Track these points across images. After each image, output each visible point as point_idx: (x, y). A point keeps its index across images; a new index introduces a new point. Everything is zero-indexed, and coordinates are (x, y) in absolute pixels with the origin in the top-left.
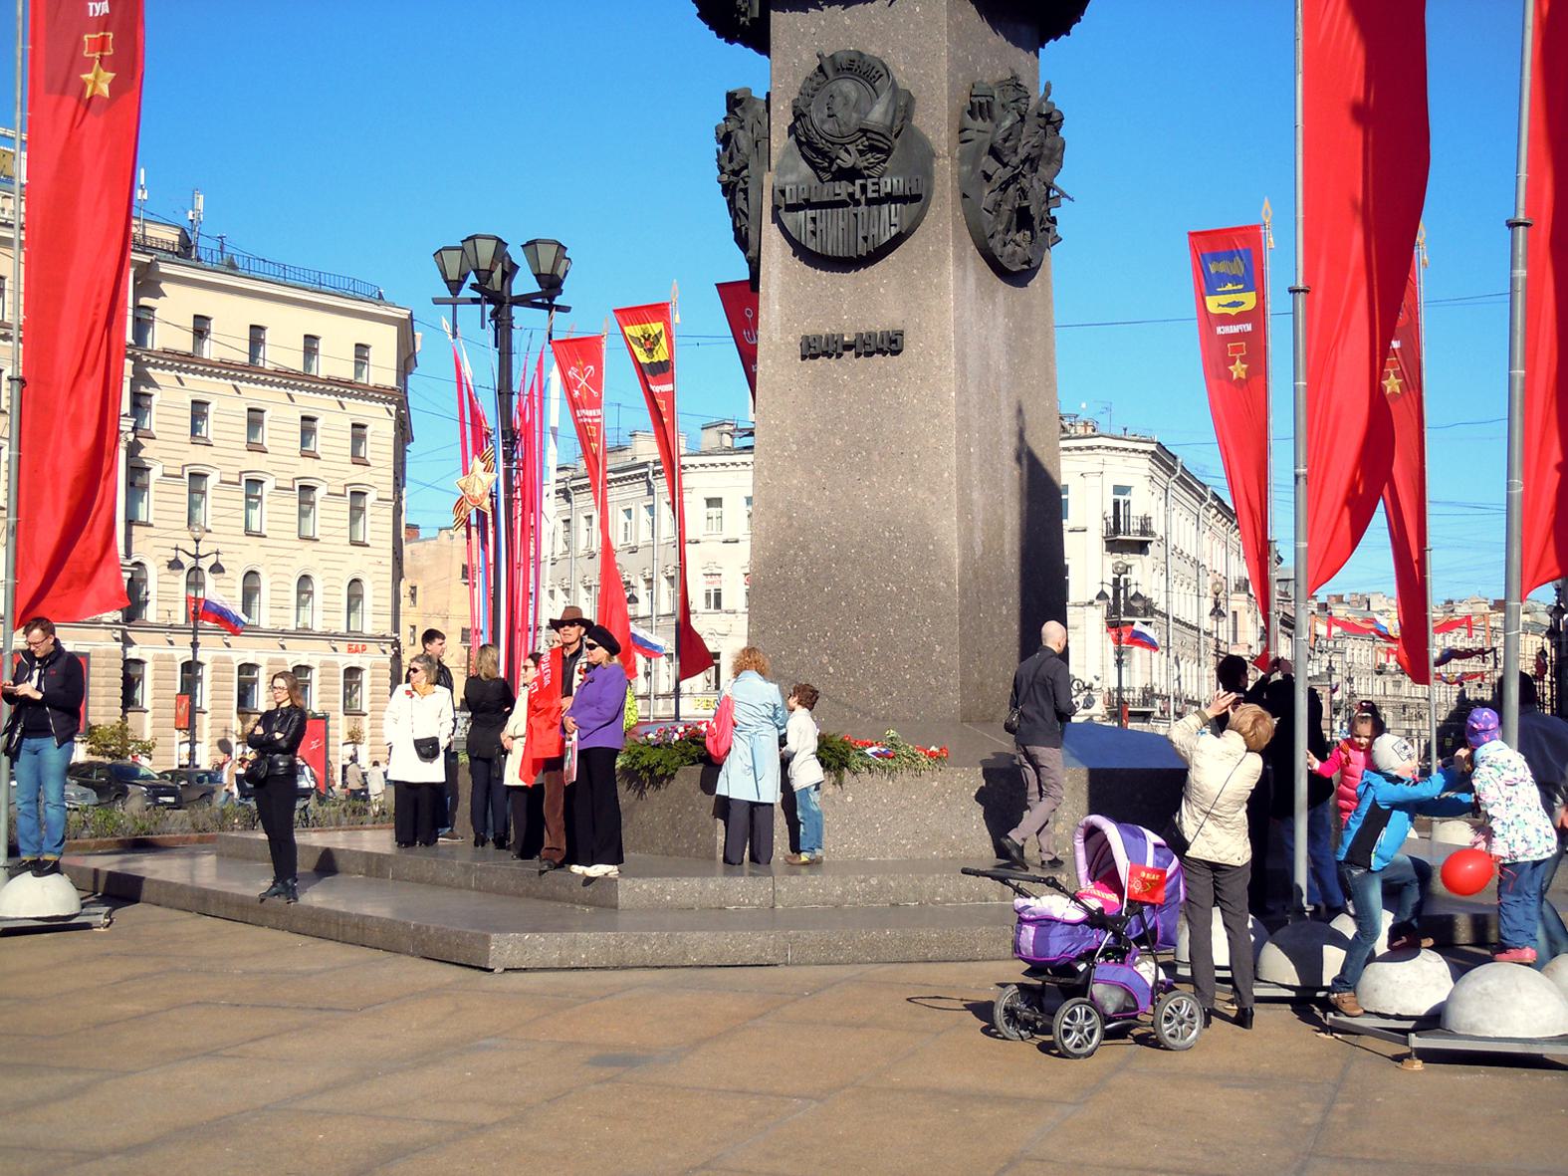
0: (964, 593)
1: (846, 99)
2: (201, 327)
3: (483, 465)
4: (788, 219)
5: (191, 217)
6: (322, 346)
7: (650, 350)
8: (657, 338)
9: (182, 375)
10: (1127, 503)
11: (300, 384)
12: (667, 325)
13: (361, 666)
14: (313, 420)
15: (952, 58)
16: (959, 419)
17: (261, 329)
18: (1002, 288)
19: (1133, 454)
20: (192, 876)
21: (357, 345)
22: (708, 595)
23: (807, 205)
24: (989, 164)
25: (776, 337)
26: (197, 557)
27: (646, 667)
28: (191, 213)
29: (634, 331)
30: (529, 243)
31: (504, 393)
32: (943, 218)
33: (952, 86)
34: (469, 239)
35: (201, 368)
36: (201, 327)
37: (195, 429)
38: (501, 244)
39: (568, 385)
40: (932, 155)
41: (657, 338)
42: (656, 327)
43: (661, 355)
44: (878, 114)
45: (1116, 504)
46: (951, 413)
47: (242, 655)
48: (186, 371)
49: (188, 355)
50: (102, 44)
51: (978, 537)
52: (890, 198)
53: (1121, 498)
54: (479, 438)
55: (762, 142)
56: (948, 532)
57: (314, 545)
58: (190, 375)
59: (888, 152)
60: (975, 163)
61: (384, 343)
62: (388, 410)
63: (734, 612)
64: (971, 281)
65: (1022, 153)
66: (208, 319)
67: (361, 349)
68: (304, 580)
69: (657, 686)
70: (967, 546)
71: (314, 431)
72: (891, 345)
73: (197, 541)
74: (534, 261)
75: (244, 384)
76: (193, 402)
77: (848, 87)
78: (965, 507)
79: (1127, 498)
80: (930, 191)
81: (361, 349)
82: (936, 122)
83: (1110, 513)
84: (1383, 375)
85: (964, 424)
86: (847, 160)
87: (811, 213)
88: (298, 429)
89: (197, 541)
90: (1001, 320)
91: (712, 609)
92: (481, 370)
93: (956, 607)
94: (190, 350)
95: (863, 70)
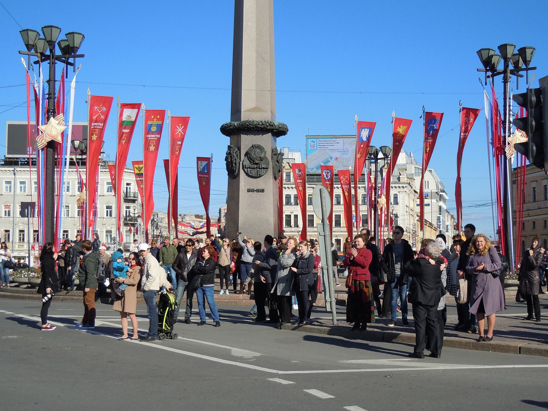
4: (246, 170)
8: (142, 168)
10: (130, 188)
20: (40, 307)
22: (5, 212)
23: (250, 168)
29: (137, 166)
32: (270, 172)
41: (142, 168)
44: (262, 155)
45: (127, 188)
52: (263, 168)
53: (128, 187)
72: (263, 191)
84: (149, 145)
86: (257, 162)
95: (259, 147)
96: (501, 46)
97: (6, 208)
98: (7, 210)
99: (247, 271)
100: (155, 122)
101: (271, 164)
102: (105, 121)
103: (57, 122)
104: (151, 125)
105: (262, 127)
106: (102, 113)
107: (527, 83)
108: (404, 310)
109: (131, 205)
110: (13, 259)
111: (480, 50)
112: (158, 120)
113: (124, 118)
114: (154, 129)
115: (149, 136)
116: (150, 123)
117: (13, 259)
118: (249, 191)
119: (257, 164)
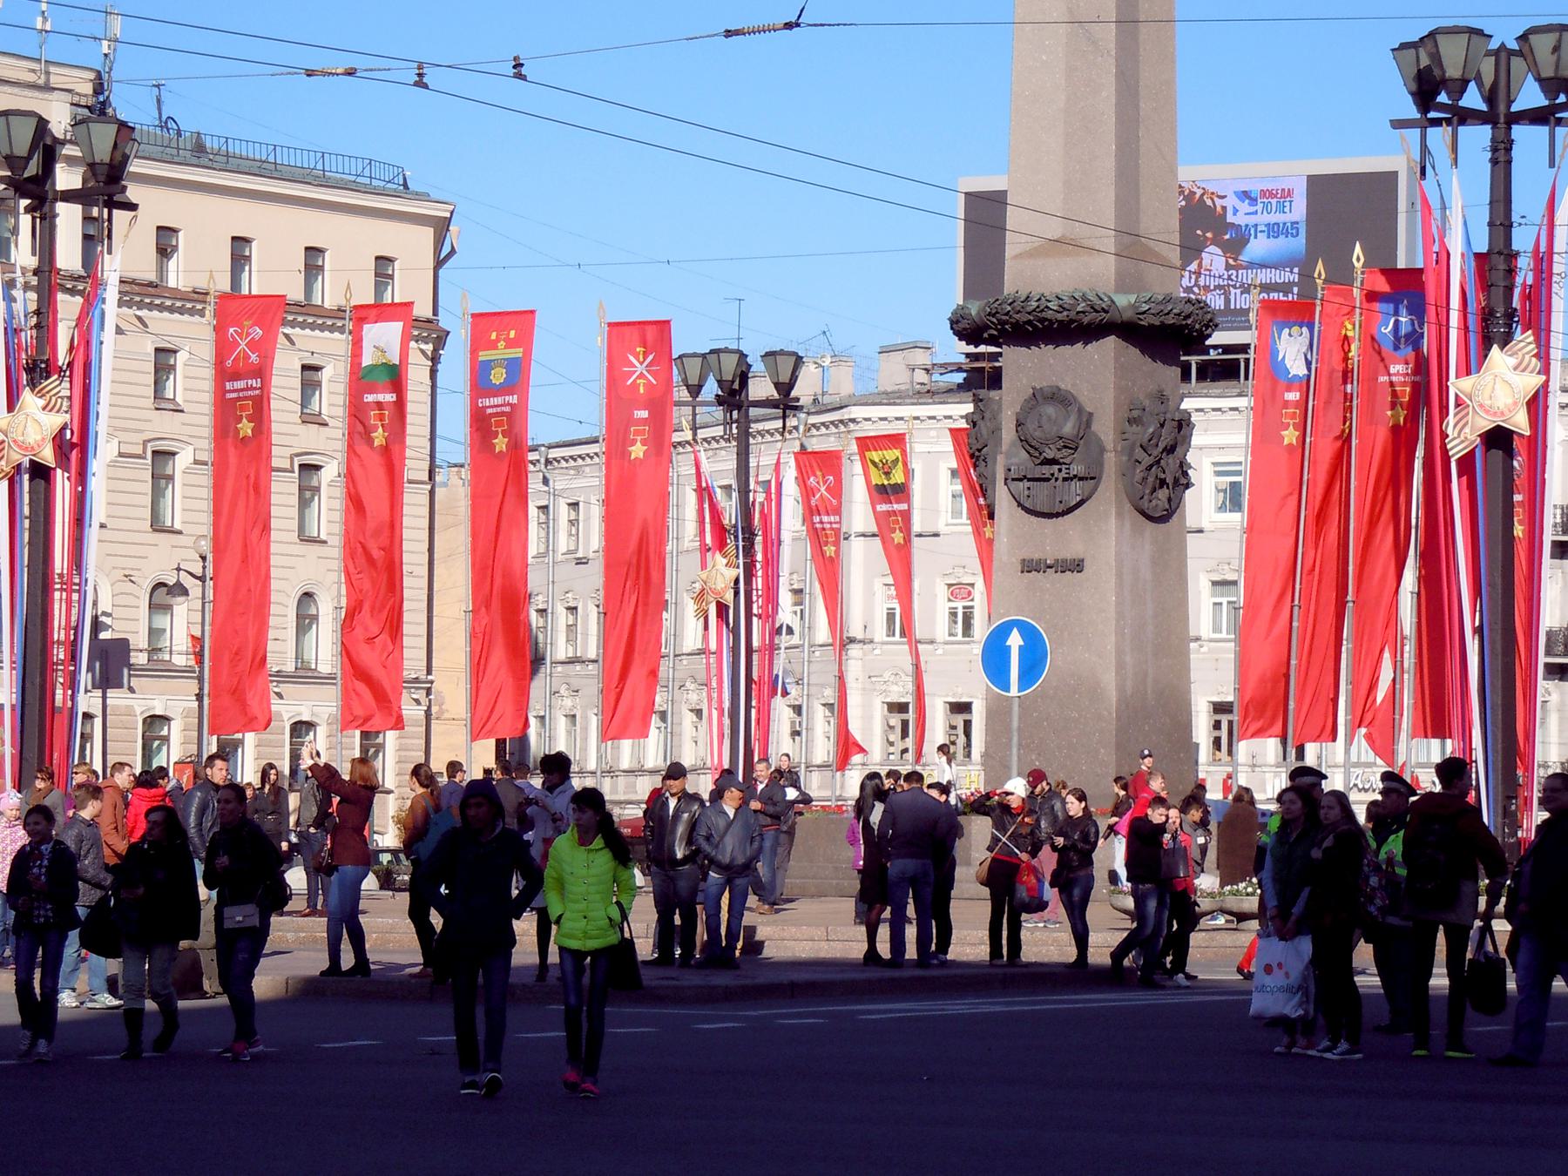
0: (1118, 718)
1: (1049, 418)
3: (725, 561)
4: (1013, 485)
5: (106, 51)
7: (887, 474)
9: (143, 313)
11: (300, 319)
12: (904, 452)
14: (317, 369)
15: (1118, 388)
16: (1117, 613)
18: (1150, 525)
21: (377, 258)
22: (954, 614)
25: (1005, 558)
27: (793, 723)
29: (875, 456)
30: (768, 354)
32: (1109, 493)
34: (712, 352)
35: (168, 303)
37: (158, 393)
38: (743, 356)
39: (807, 492)
43: (898, 477)
44: (1068, 428)
48: (151, 307)
49: (150, 284)
51: (1129, 683)
55: (996, 431)
56: (1109, 682)
57: (316, 548)
58: (155, 313)
59: (1076, 449)
60: (1131, 455)
61: (412, 247)
62: (423, 352)
63: (932, 642)
64: (1127, 525)
65: (1161, 446)
66: (174, 231)
68: (307, 599)
70: (1121, 689)
71: (318, 384)
72: (1077, 566)
74: (773, 372)
76: (157, 350)
77: (1050, 410)
78: (1120, 666)
80: (1101, 472)
81: (383, 262)
82: (1105, 428)
85: (1120, 615)
86: (1049, 454)
87: (1027, 484)
88: (297, 383)
90: (1148, 547)
91: (897, 638)
92: (720, 466)
93: (1113, 727)
96: (1404, 46)
97: (953, 596)
98: (960, 605)
99: (706, 898)
101: (1110, 460)
103: (42, 402)
105: (1060, 317)
106: (253, 345)
107: (1552, 164)
110: (593, 871)
111: (1432, 35)
112: (511, 344)
116: (484, 356)
117: (593, 871)
118: (1030, 566)
119: (1053, 462)
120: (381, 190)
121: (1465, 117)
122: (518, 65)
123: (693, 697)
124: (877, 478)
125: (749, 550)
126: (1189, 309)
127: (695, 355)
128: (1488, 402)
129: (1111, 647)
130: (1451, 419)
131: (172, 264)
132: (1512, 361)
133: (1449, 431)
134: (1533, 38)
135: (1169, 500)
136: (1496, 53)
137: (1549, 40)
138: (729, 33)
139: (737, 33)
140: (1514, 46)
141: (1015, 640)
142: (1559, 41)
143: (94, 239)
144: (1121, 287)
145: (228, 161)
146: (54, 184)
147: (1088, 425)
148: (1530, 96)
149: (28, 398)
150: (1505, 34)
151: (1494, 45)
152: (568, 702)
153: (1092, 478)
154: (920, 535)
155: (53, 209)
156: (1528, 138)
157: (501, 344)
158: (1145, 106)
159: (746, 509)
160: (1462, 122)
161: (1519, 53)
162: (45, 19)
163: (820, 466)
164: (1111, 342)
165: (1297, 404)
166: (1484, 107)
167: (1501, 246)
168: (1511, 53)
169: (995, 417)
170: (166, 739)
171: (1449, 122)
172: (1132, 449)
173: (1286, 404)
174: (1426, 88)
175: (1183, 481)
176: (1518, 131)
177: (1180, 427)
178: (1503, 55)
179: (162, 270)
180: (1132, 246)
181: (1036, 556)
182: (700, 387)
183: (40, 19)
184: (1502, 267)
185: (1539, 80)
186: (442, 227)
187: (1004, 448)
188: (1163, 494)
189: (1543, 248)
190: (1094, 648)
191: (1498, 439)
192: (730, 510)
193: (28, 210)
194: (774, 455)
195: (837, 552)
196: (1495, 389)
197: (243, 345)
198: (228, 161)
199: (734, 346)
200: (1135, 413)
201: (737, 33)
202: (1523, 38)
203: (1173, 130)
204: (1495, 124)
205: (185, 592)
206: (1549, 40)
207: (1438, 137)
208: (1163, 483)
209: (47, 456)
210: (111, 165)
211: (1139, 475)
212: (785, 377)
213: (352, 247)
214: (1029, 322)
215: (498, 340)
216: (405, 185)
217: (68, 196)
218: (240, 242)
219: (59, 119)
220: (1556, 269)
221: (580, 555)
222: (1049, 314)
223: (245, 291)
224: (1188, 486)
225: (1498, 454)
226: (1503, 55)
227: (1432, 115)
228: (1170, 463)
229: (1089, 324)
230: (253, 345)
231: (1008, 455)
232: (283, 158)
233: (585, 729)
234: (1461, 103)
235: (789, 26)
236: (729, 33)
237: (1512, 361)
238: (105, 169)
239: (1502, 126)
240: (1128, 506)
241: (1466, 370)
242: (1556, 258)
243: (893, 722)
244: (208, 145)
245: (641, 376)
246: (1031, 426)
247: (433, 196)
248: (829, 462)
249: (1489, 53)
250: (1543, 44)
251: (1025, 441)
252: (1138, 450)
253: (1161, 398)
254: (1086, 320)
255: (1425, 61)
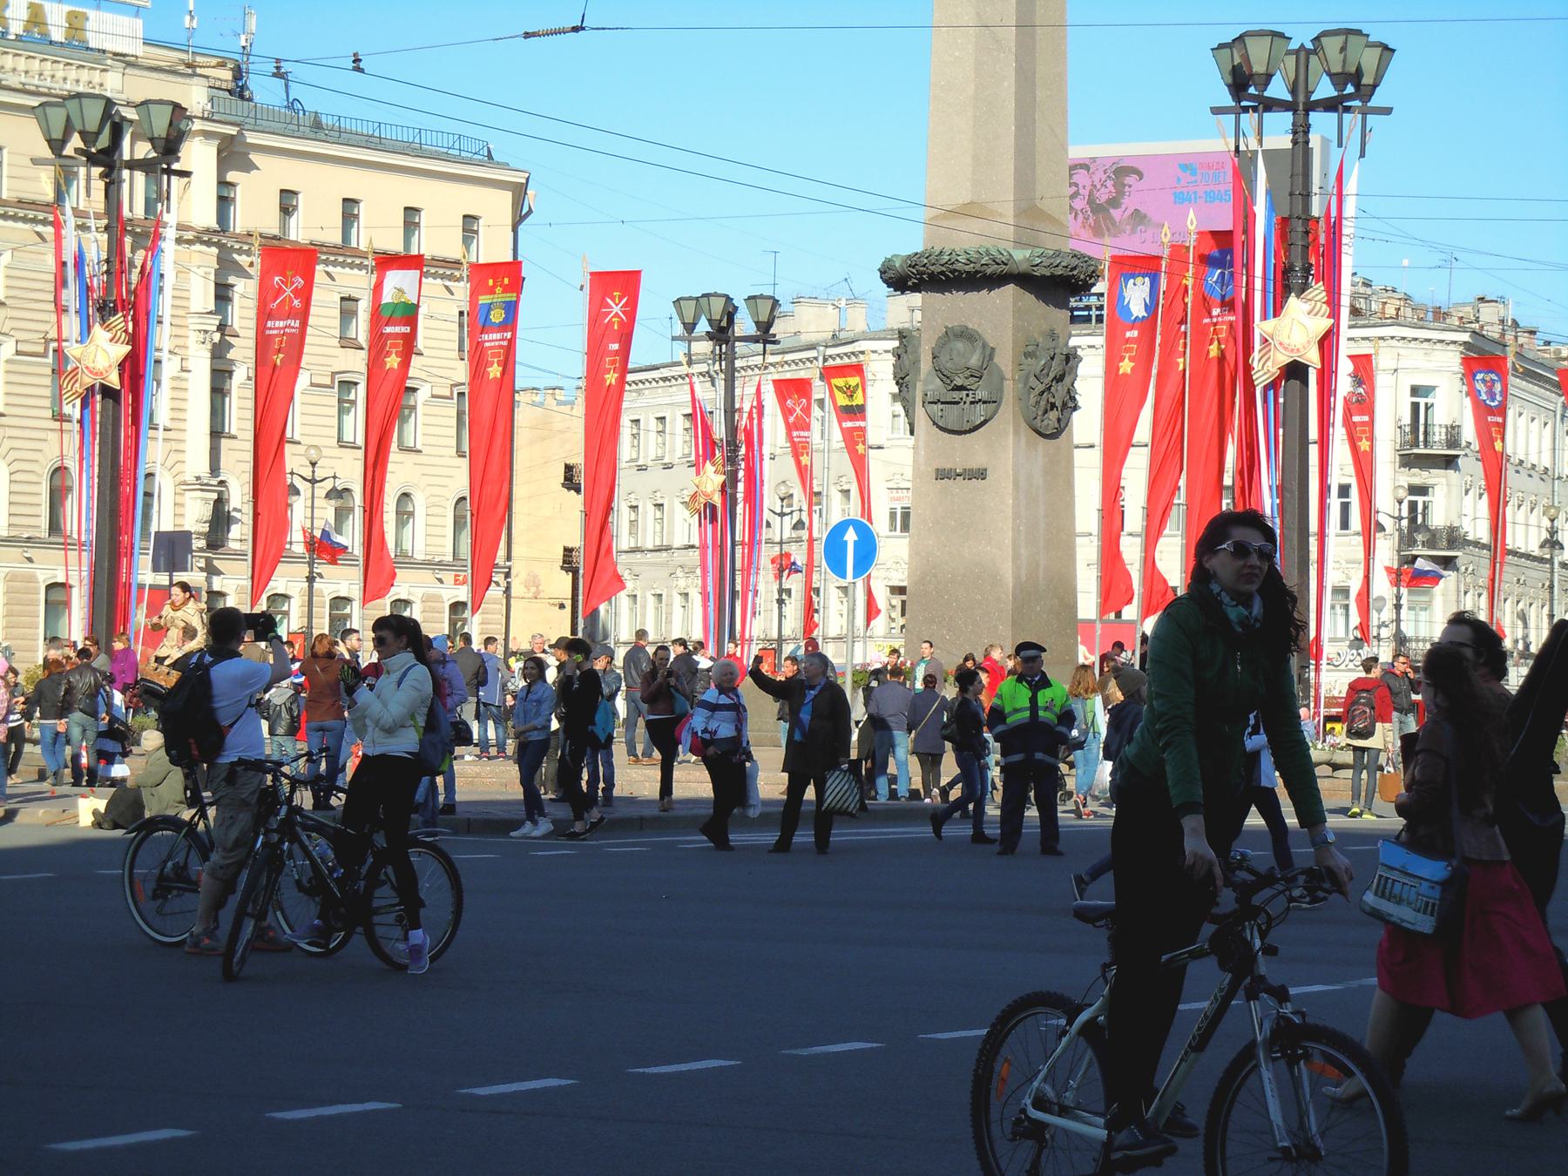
2: (287, 202)
6: (424, 219)
13: (411, 598)
17: (355, 202)
19: (1439, 346)
22: (893, 515)
24: (1033, 382)
26: (313, 481)
28: (243, 37)
29: (839, 382)
31: (730, 410)
32: (1007, 412)
33: (1015, 343)
34: (704, 296)
36: (287, 202)
38: (728, 299)
39: (787, 412)
40: (1003, 378)
42: (854, 381)
43: (858, 400)
44: (974, 361)
45: (1415, 406)
46: (1009, 511)
47: (335, 587)
50: (613, 362)
53: (1422, 401)
54: (708, 447)
57: (413, 456)
61: (495, 207)
64: (1023, 441)
65: (1052, 376)
66: (295, 193)
67: (469, 220)
69: (671, 533)
70: (1016, 577)
72: (981, 474)
73: (313, 464)
74: (754, 313)
75: (339, 269)
77: (959, 345)
78: (1016, 557)
79: (1429, 400)
81: (469, 220)
82: (1005, 361)
83: (1407, 419)
85: (1016, 516)
86: (958, 382)
89: (313, 464)
91: (898, 532)
93: (1009, 607)
94: (276, 232)
95: (966, 335)
96: (1221, 46)
100: (500, 297)
101: (1009, 388)
102: (304, 315)
103: (110, 335)
104: (489, 307)
105: (967, 268)
106: (297, 292)
108: (930, 761)
109: (1436, 478)
111: (1241, 38)
113: (388, 297)
114: (497, 316)
115: (485, 337)
116: (484, 300)
120: (467, 161)
121: (1270, 105)
122: (357, 60)
123: (682, 583)
124: (842, 400)
125: (732, 459)
126: (1075, 262)
127: (690, 298)
128: (1286, 341)
129: (1008, 542)
130: (1256, 355)
131: (293, 220)
132: (1308, 307)
133: (1255, 365)
134: (1324, 40)
135: (1059, 420)
136: (1297, 52)
137: (1338, 41)
138: (527, 35)
139: (534, 35)
140: (1310, 46)
141: (851, 536)
142: (1346, 42)
143: (157, 199)
144: (1018, 244)
145: (340, 136)
146: (121, 155)
147: (991, 357)
148: (1324, 89)
149: (97, 329)
150: (1302, 37)
151: (1294, 45)
152: (682, 583)
153: (993, 402)
154: (1092, 446)
155: (120, 176)
156: (1323, 124)
157: (498, 290)
158: (1041, 94)
159: (732, 429)
160: (1268, 109)
161: (1315, 52)
162: (192, 17)
163: (794, 390)
164: (1010, 288)
165: (616, 353)
166: (1289, 98)
167: (1299, 210)
168: (1309, 52)
169: (916, 352)
170: (286, 614)
171: (1255, 109)
172: (1027, 377)
173: (1128, 340)
174: (1241, 82)
175: (1071, 404)
176: (1316, 118)
177: (1068, 358)
178: (1302, 54)
179: (284, 226)
180: (1029, 211)
181: (948, 466)
182: (694, 325)
183: (188, 18)
184: (1300, 229)
185: (1330, 75)
186: (519, 192)
187: (922, 376)
188: (1053, 415)
189: (1334, 213)
190: (997, 545)
191: (1295, 371)
192: (719, 431)
193: (102, 176)
194: (757, 382)
195: (1372, 447)
196: (1293, 330)
197: (288, 291)
198: (340, 136)
199: (768, 292)
200: (1030, 349)
201: (534, 35)
202: (1316, 40)
203: (1064, 113)
204: (1295, 111)
205: (297, 493)
206: (1338, 41)
207: (1249, 120)
208: (1053, 406)
209: (114, 380)
210: (167, 140)
211: (1033, 400)
212: (764, 318)
213: (445, 208)
214: (942, 273)
215: (495, 286)
216: (490, 156)
217: (133, 165)
218: (350, 203)
219: (195, 97)
220: (1345, 231)
221: (666, 460)
222: (958, 266)
223: (354, 244)
224: (1075, 408)
225: (1295, 384)
226: (1302, 54)
227: (1244, 103)
228: (1059, 391)
229: (992, 275)
230: (297, 292)
231: (926, 382)
232: (387, 133)
233: (644, 607)
234: (1266, 94)
235: (575, 29)
236: (527, 35)
237: (1308, 307)
238: (162, 143)
239: (1301, 112)
240: (1025, 429)
241: (1265, 317)
242: (1345, 222)
243: (894, 602)
244: (324, 121)
245: (617, 315)
246: (944, 358)
247: (512, 166)
248: (800, 388)
249: (1289, 53)
250: (1332, 46)
251: (939, 371)
252: (1032, 379)
253: (1053, 336)
254: (989, 271)
255: (1237, 60)
